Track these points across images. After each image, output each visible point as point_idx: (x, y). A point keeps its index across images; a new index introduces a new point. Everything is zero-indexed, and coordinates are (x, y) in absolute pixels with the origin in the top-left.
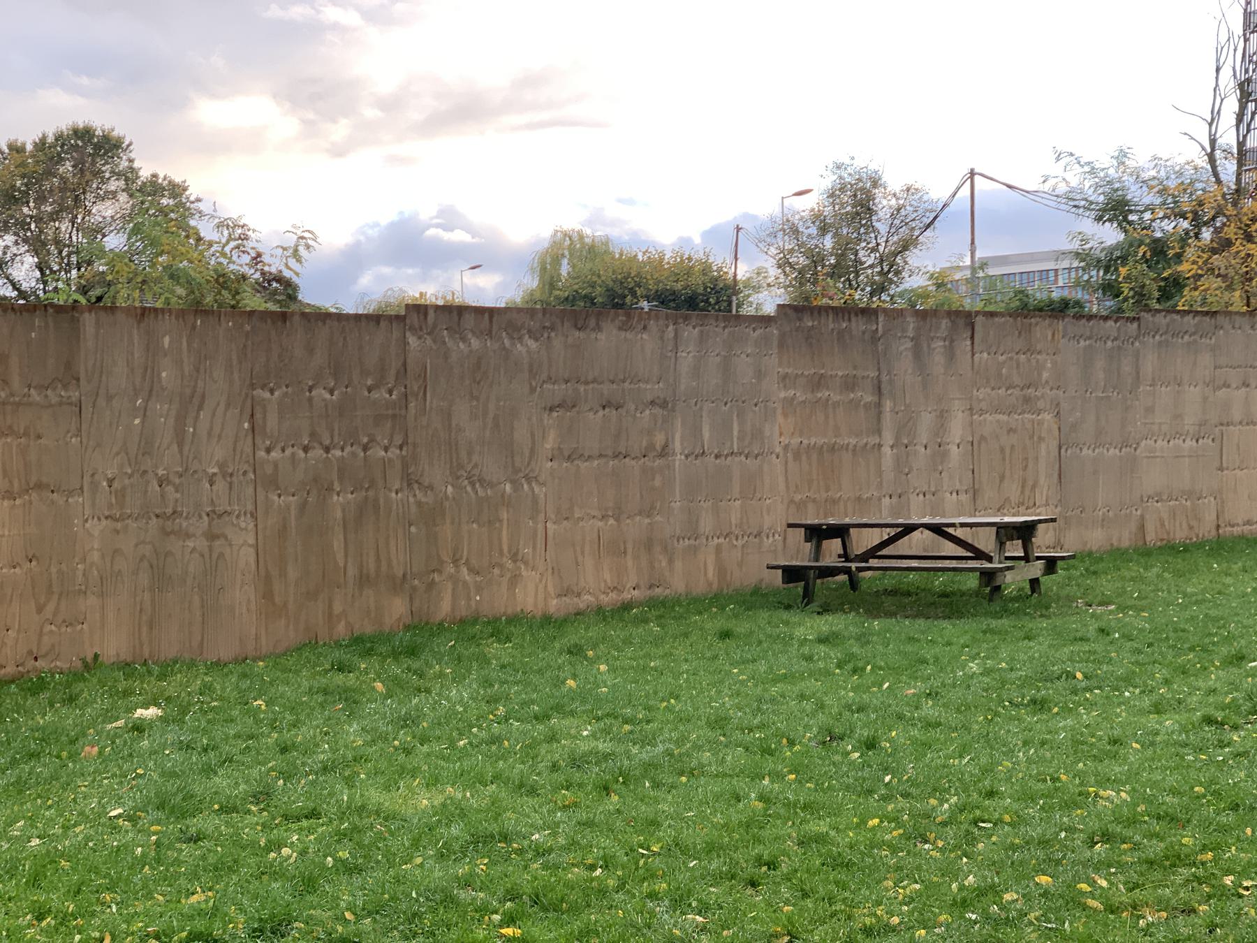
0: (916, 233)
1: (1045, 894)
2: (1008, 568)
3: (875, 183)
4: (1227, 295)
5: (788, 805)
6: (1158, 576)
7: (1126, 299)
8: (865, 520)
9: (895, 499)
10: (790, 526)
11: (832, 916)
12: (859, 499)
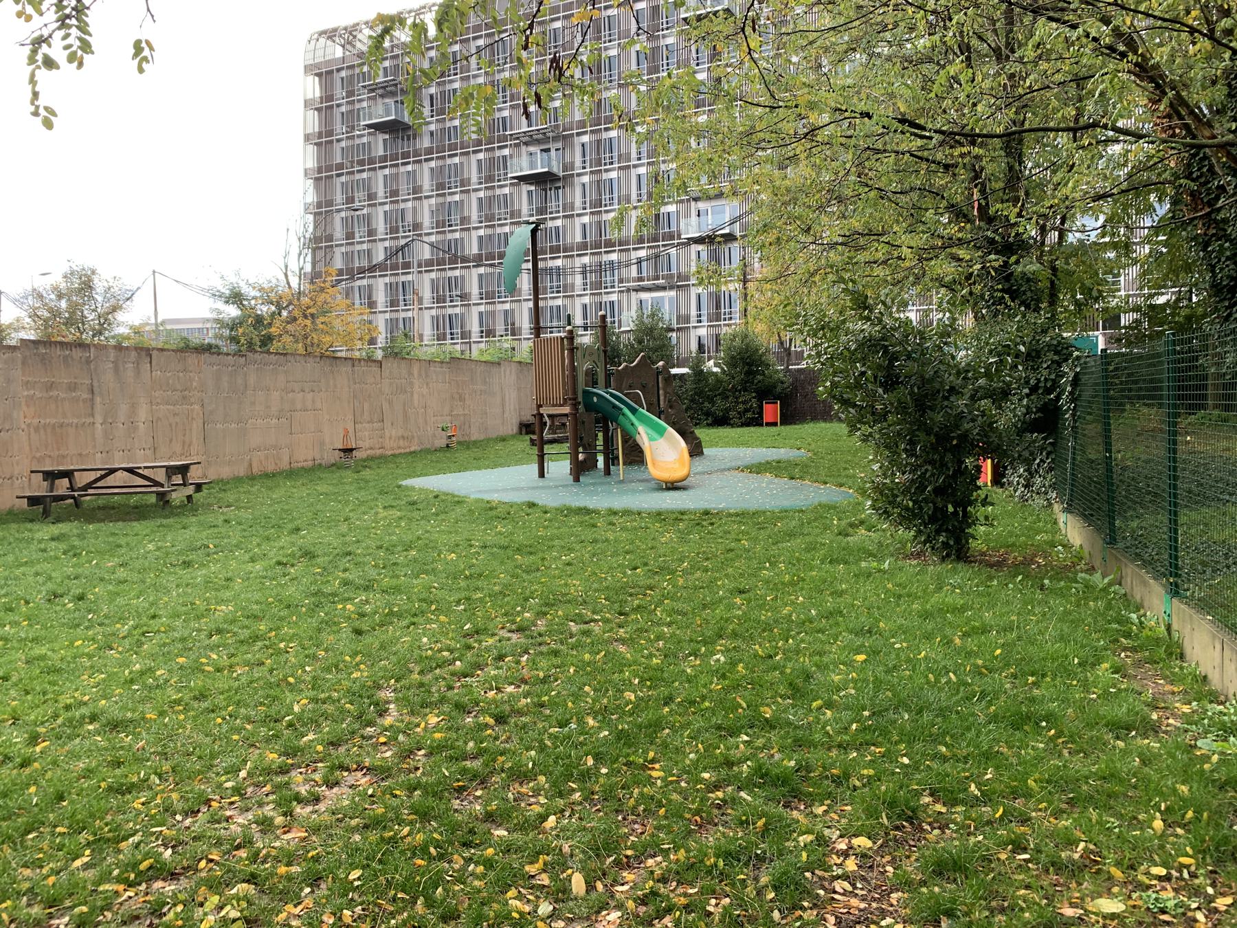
0: (121, 302)
1: (181, 668)
2: (173, 491)
3: (93, 272)
5: (21, 640)
7: (243, 345)
8: (84, 467)
9: (104, 454)
10: (32, 472)
11: (44, 702)
12: (80, 455)
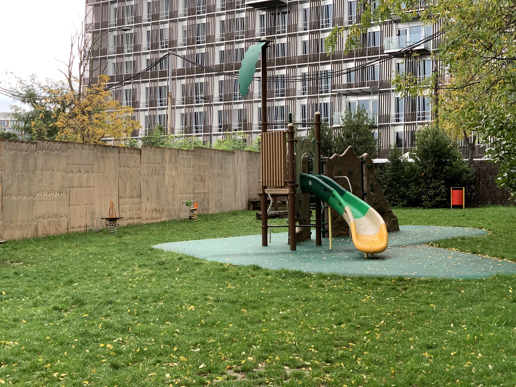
4: (75, 136)
6: (42, 249)
7: (34, 135)
